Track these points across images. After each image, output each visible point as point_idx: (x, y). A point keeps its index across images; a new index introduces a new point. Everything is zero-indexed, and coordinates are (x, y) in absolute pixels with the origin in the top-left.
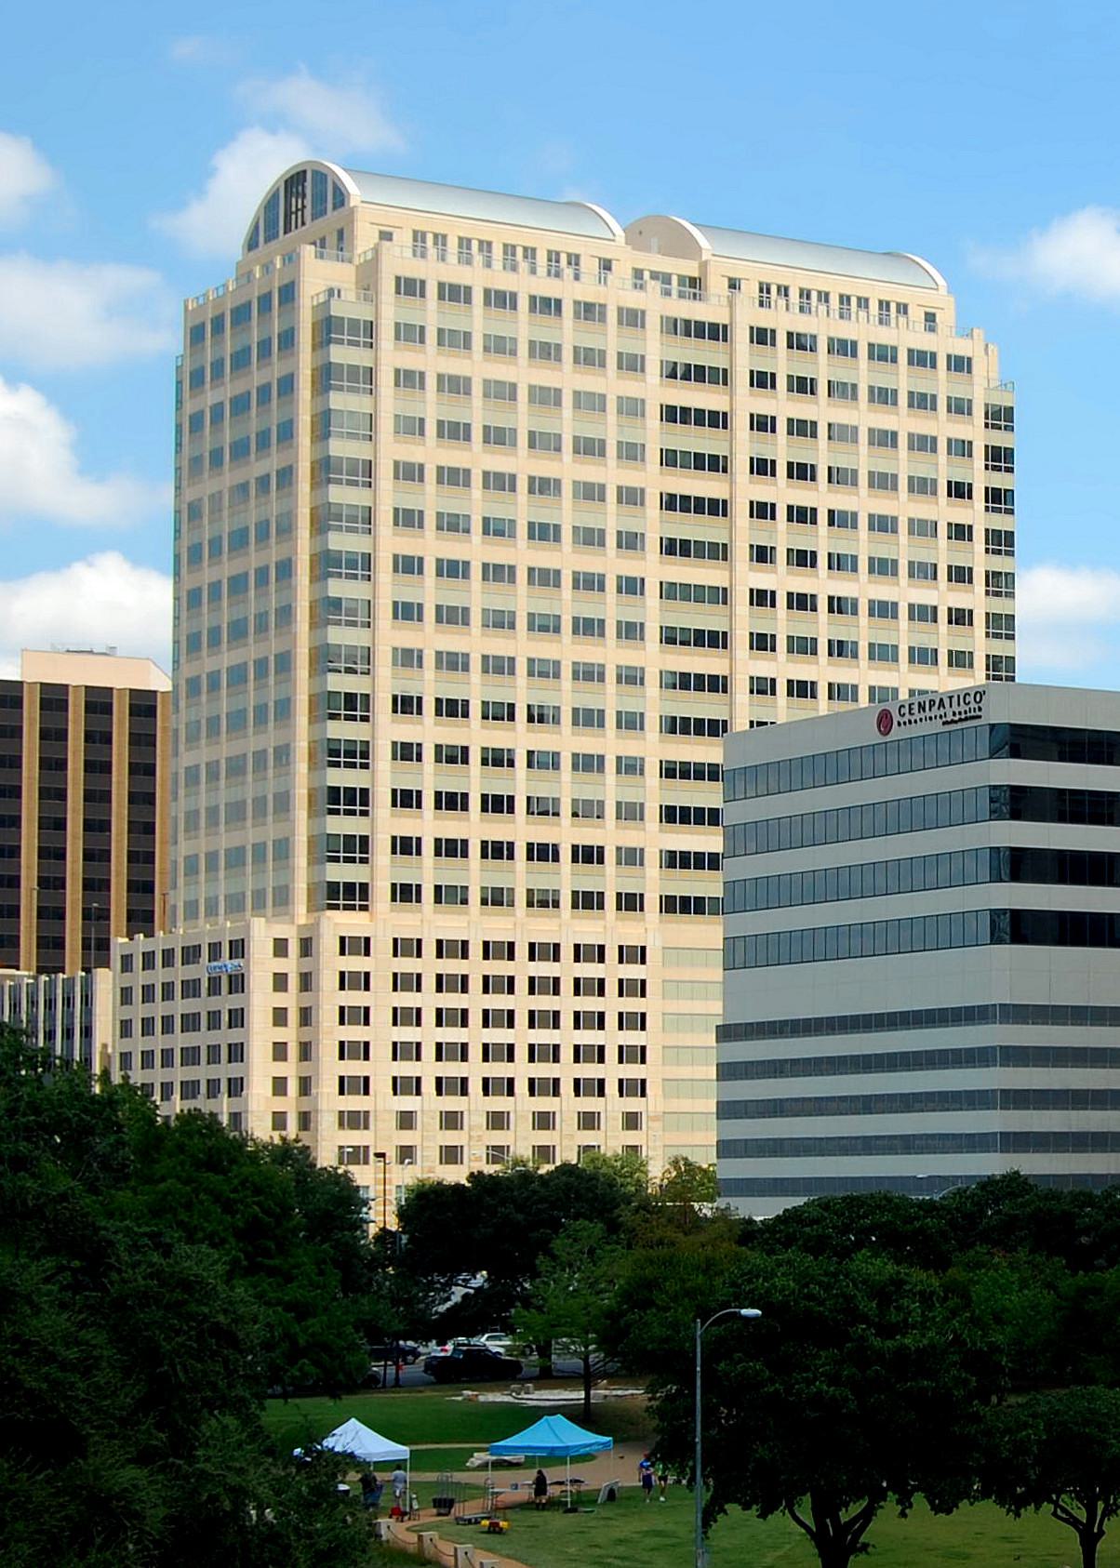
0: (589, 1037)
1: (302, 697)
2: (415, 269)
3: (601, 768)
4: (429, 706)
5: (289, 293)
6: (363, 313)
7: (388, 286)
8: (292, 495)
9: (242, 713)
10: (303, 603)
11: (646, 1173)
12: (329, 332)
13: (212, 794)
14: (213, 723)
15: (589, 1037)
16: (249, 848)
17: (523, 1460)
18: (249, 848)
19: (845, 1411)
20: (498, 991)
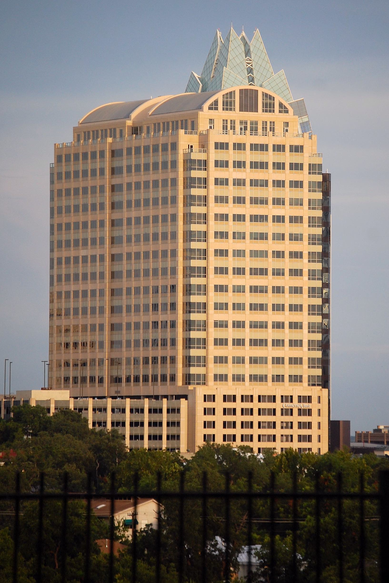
0: (247, 418)
1: (181, 214)
2: (223, 139)
3: (243, 362)
4: (248, 201)
5: (175, 146)
6: (202, 156)
7: (212, 146)
8: (176, 243)
9: (166, 304)
10: (181, 214)
11: (219, 444)
12: (190, 344)
13: (137, 264)
14: (138, 237)
15: (247, 418)
16: (142, 218)
17: (255, 534)
18: (142, 218)
19: (228, 466)
20: (229, 409)
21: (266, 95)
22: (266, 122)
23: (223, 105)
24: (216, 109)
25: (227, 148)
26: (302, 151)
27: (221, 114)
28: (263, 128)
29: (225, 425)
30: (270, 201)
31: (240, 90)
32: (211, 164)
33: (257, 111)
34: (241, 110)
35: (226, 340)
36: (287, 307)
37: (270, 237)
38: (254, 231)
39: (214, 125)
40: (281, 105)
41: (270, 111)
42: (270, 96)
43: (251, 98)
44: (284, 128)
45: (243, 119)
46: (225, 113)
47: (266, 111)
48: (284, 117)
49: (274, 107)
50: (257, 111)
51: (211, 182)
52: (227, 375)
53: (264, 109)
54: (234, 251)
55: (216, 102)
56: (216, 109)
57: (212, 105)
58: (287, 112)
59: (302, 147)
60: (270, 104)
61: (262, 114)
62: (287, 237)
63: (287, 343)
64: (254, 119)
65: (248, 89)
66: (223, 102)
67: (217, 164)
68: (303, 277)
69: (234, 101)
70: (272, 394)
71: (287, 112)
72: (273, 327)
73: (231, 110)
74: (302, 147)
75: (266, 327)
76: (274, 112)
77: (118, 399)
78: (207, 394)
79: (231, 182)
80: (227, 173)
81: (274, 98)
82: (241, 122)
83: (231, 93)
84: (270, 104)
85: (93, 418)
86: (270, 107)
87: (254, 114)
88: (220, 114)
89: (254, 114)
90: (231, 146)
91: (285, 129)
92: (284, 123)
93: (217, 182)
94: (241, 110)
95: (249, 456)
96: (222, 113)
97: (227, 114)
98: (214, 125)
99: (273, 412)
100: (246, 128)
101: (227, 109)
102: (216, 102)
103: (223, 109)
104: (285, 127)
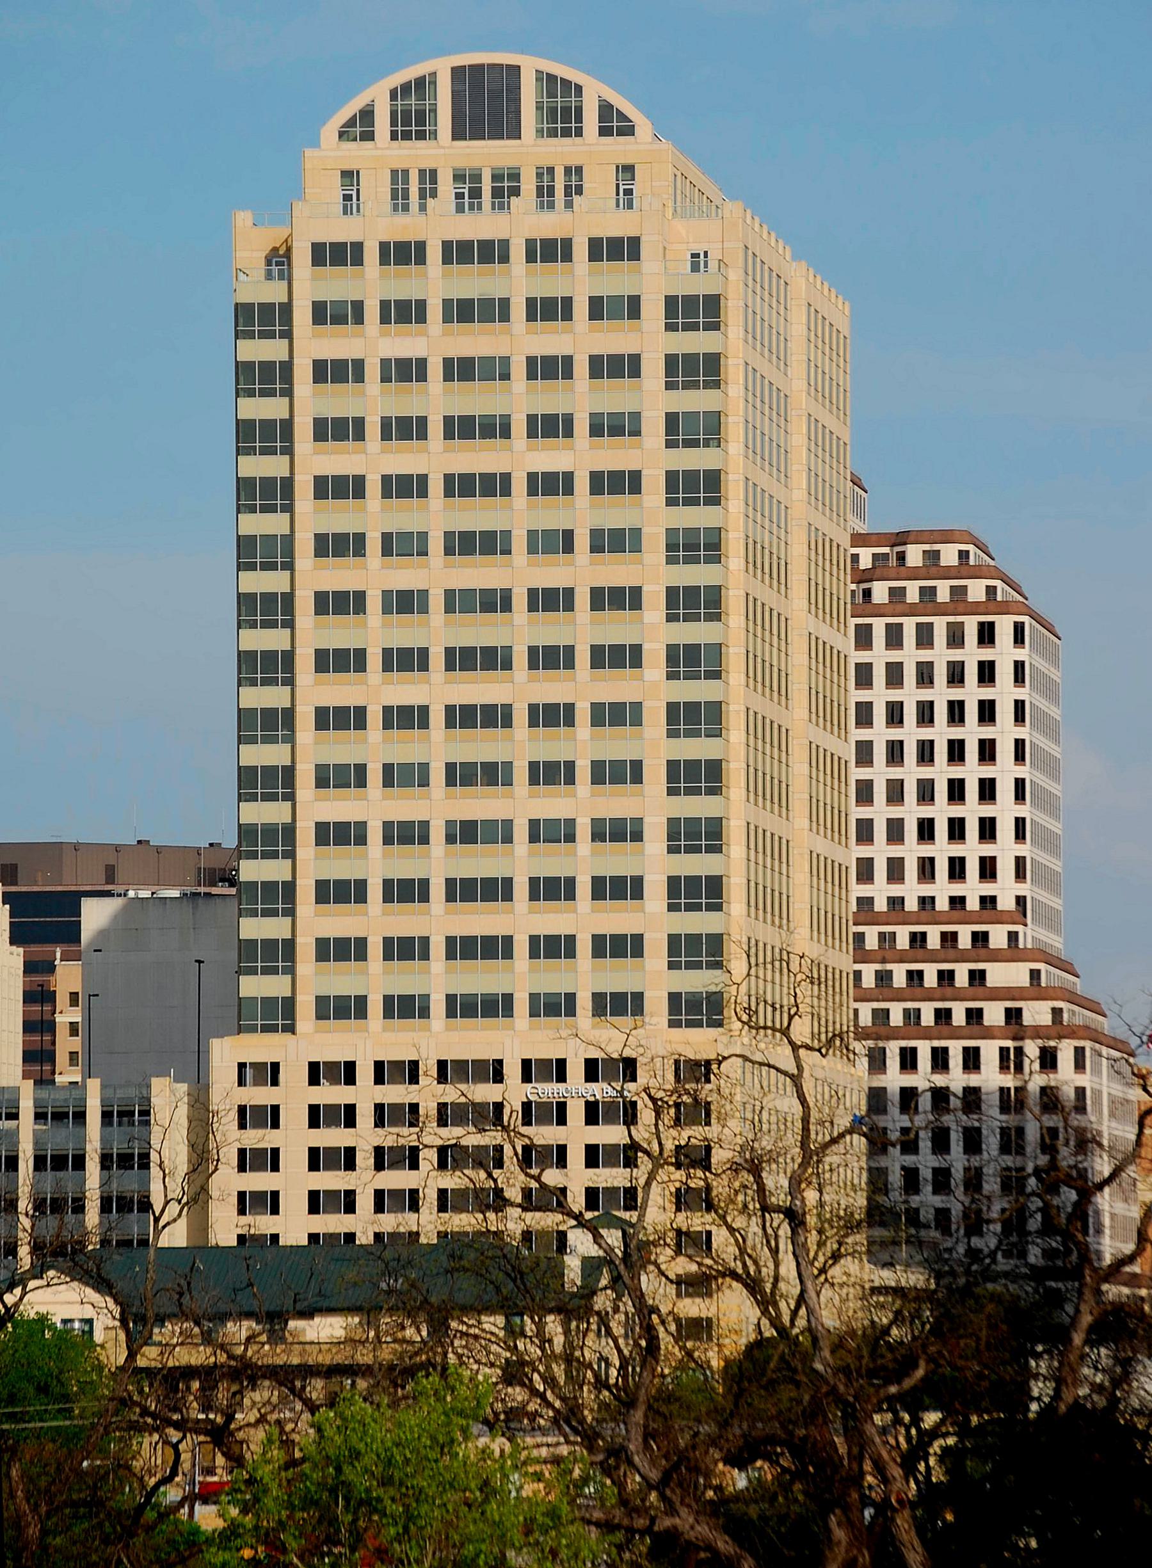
2: (342, 231)
6: (274, 293)
21: (551, 78)
22: (406, 172)
23: (394, 123)
24: (368, 136)
25: (421, 260)
26: (635, 255)
27: (388, 152)
28: (540, 189)
29: (316, 1158)
30: (519, 427)
31: (453, 69)
32: (302, 316)
33: (515, 133)
34: (457, 135)
35: (425, 884)
36: (583, 772)
37: (519, 543)
38: (540, 526)
39: (358, 190)
40: (606, 110)
41: (566, 133)
42: (566, 83)
43: (495, 95)
44: (618, 186)
45: (463, 163)
46: (400, 148)
47: (553, 133)
48: (618, 149)
49: (579, 119)
50: (515, 133)
51: (303, 373)
52: (429, 995)
53: (545, 126)
54: (386, 594)
55: (367, 115)
56: (368, 136)
57: (351, 123)
58: (628, 130)
59: (635, 242)
60: (566, 110)
61: (451, 147)
62: (582, 541)
63: (437, 890)
64: (428, 165)
65: (483, 65)
66: (393, 114)
67: (321, 313)
68: (642, 672)
69: (434, 111)
70: (491, 1055)
71: (628, 130)
72: (387, 840)
73: (421, 136)
74: (635, 242)
75: (425, 840)
76: (579, 133)
77: (758, 1057)
78: (247, 1059)
79: (373, 371)
80: (567, 337)
81: (579, 89)
82: (459, 177)
83: (420, 82)
84: (566, 110)
85: (103, 1140)
86: (566, 119)
87: (468, 147)
88: (379, 152)
89: (468, 147)
90: (371, 254)
91: (622, 188)
92: (617, 167)
93: (324, 371)
94: (457, 135)
95: (1012, 1235)
96: (597, 144)
97: (405, 152)
98: (358, 190)
99: (349, 1115)
100: (476, 193)
101: (407, 136)
102: (367, 115)
103: (394, 136)
104: (621, 183)
